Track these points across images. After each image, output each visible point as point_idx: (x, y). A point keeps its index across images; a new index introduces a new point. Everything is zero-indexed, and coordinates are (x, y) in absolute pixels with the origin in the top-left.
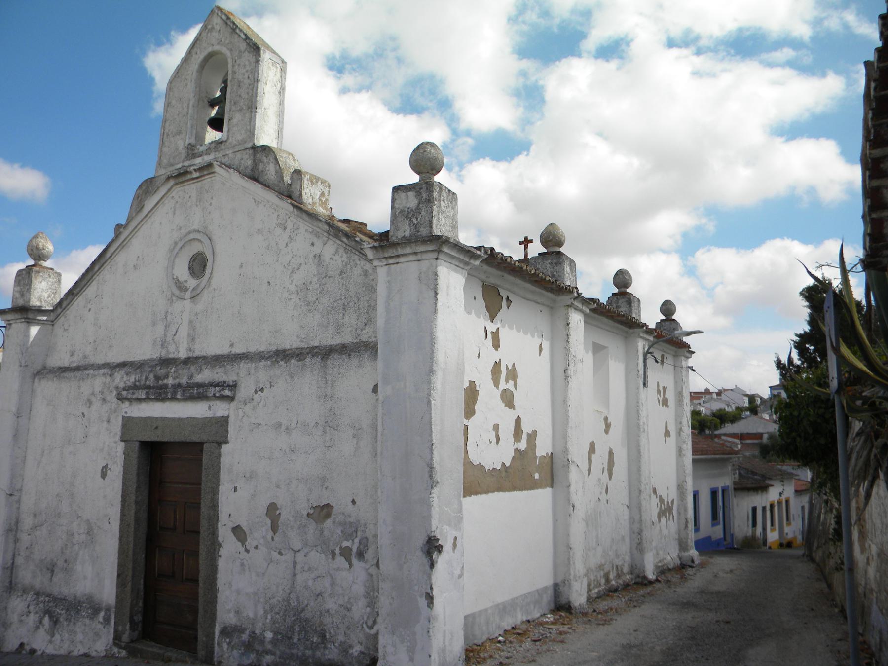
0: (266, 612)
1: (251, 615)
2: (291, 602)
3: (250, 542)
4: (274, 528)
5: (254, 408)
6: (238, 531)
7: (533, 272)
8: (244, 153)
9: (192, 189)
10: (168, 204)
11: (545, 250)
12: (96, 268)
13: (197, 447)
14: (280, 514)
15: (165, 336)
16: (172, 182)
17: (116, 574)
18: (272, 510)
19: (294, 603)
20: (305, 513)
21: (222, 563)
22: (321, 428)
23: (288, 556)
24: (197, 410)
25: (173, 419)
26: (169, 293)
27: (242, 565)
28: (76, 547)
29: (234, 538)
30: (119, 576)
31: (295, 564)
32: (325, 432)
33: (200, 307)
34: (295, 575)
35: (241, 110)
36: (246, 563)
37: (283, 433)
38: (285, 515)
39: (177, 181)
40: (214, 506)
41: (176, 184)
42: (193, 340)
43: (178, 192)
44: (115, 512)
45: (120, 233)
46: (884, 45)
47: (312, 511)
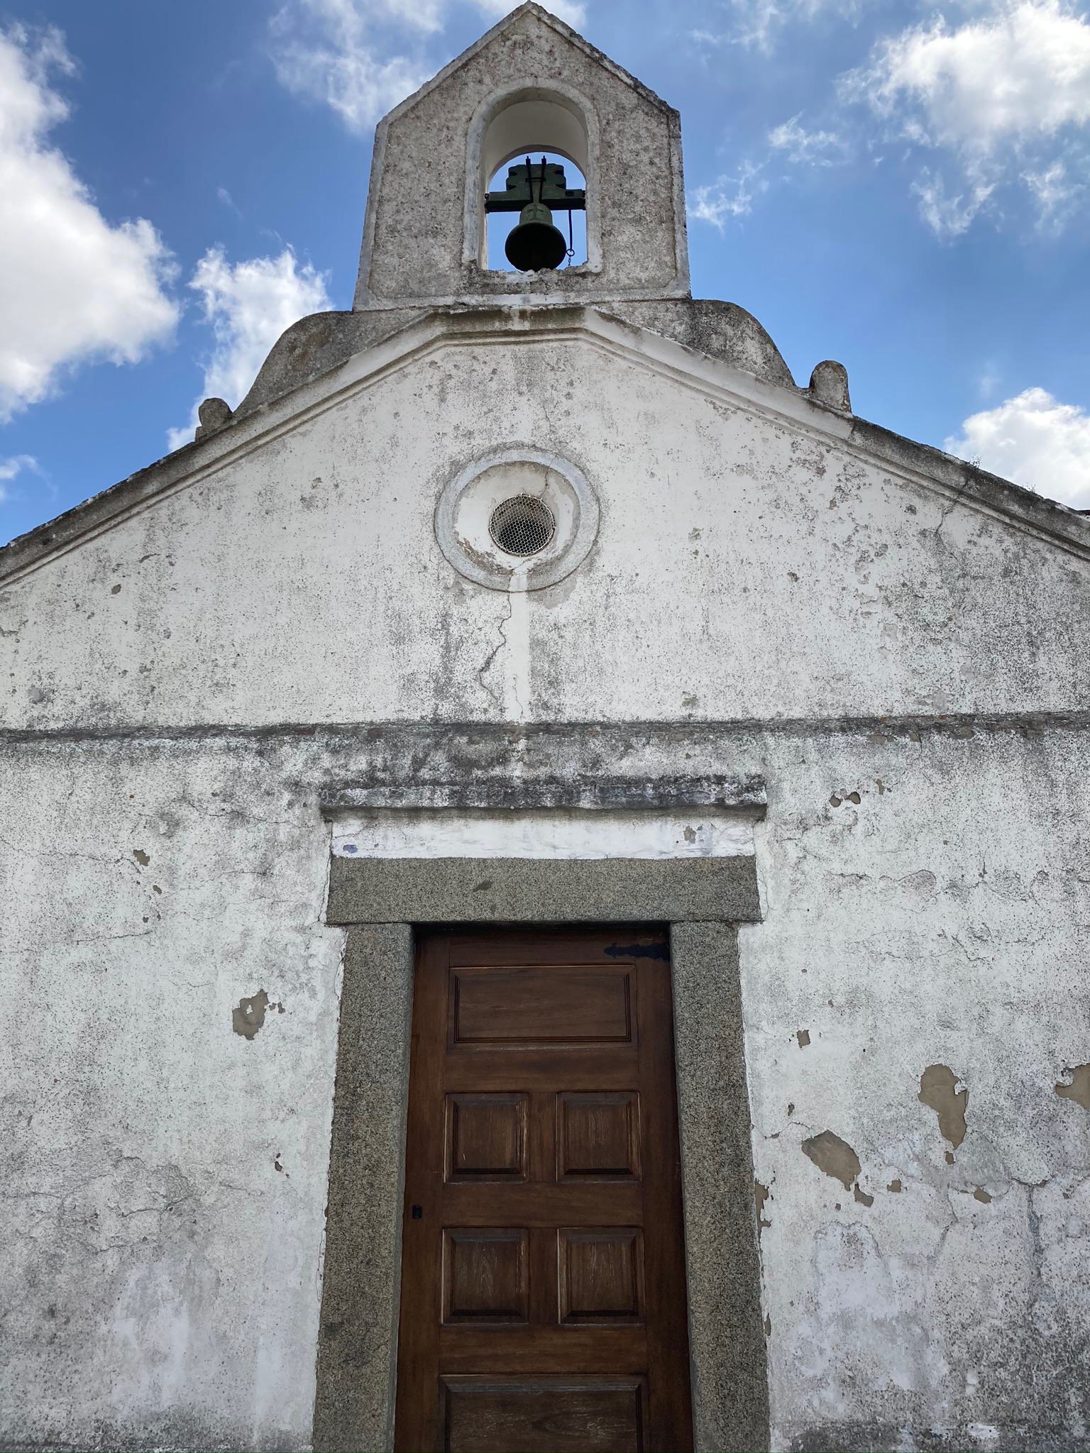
0: (955, 1366)
1: (904, 1382)
2: (1041, 1326)
3: (871, 1175)
4: (953, 1128)
5: (835, 839)
6: (827, 1151)
8: (661, 307)
9: (502, 359)
10: (419, 377)
12: (151, 488)
13: (651, 939)
14: (965, 1091)
16: (439, 329)
17: (312, 1327)
18: (940, 1087)
19: (1049, 1330)
20: (1047, 1085)
21: (773, 1246)
22: (1058, 885)
23: (1012, 1200)
24: (656, 840)
25: (553, 865)
27: (852, 1240)
28: (111, 1260)
29: (813, 1170)
30: (329, 1330)
31: (1035, 1222)
32: (1071, 894)
33: (563, 612)
34: (1039, 1250)
35: (638, 220)
36: (863, 1234)
37: (942, 897)
38: (981, 1094)
39: (456, 329)
40: (732, 1087)
42: (554, 683)
43: (452, 357)
44: (307, 1138)
45: (257, 414)
47: (1068, 1080)
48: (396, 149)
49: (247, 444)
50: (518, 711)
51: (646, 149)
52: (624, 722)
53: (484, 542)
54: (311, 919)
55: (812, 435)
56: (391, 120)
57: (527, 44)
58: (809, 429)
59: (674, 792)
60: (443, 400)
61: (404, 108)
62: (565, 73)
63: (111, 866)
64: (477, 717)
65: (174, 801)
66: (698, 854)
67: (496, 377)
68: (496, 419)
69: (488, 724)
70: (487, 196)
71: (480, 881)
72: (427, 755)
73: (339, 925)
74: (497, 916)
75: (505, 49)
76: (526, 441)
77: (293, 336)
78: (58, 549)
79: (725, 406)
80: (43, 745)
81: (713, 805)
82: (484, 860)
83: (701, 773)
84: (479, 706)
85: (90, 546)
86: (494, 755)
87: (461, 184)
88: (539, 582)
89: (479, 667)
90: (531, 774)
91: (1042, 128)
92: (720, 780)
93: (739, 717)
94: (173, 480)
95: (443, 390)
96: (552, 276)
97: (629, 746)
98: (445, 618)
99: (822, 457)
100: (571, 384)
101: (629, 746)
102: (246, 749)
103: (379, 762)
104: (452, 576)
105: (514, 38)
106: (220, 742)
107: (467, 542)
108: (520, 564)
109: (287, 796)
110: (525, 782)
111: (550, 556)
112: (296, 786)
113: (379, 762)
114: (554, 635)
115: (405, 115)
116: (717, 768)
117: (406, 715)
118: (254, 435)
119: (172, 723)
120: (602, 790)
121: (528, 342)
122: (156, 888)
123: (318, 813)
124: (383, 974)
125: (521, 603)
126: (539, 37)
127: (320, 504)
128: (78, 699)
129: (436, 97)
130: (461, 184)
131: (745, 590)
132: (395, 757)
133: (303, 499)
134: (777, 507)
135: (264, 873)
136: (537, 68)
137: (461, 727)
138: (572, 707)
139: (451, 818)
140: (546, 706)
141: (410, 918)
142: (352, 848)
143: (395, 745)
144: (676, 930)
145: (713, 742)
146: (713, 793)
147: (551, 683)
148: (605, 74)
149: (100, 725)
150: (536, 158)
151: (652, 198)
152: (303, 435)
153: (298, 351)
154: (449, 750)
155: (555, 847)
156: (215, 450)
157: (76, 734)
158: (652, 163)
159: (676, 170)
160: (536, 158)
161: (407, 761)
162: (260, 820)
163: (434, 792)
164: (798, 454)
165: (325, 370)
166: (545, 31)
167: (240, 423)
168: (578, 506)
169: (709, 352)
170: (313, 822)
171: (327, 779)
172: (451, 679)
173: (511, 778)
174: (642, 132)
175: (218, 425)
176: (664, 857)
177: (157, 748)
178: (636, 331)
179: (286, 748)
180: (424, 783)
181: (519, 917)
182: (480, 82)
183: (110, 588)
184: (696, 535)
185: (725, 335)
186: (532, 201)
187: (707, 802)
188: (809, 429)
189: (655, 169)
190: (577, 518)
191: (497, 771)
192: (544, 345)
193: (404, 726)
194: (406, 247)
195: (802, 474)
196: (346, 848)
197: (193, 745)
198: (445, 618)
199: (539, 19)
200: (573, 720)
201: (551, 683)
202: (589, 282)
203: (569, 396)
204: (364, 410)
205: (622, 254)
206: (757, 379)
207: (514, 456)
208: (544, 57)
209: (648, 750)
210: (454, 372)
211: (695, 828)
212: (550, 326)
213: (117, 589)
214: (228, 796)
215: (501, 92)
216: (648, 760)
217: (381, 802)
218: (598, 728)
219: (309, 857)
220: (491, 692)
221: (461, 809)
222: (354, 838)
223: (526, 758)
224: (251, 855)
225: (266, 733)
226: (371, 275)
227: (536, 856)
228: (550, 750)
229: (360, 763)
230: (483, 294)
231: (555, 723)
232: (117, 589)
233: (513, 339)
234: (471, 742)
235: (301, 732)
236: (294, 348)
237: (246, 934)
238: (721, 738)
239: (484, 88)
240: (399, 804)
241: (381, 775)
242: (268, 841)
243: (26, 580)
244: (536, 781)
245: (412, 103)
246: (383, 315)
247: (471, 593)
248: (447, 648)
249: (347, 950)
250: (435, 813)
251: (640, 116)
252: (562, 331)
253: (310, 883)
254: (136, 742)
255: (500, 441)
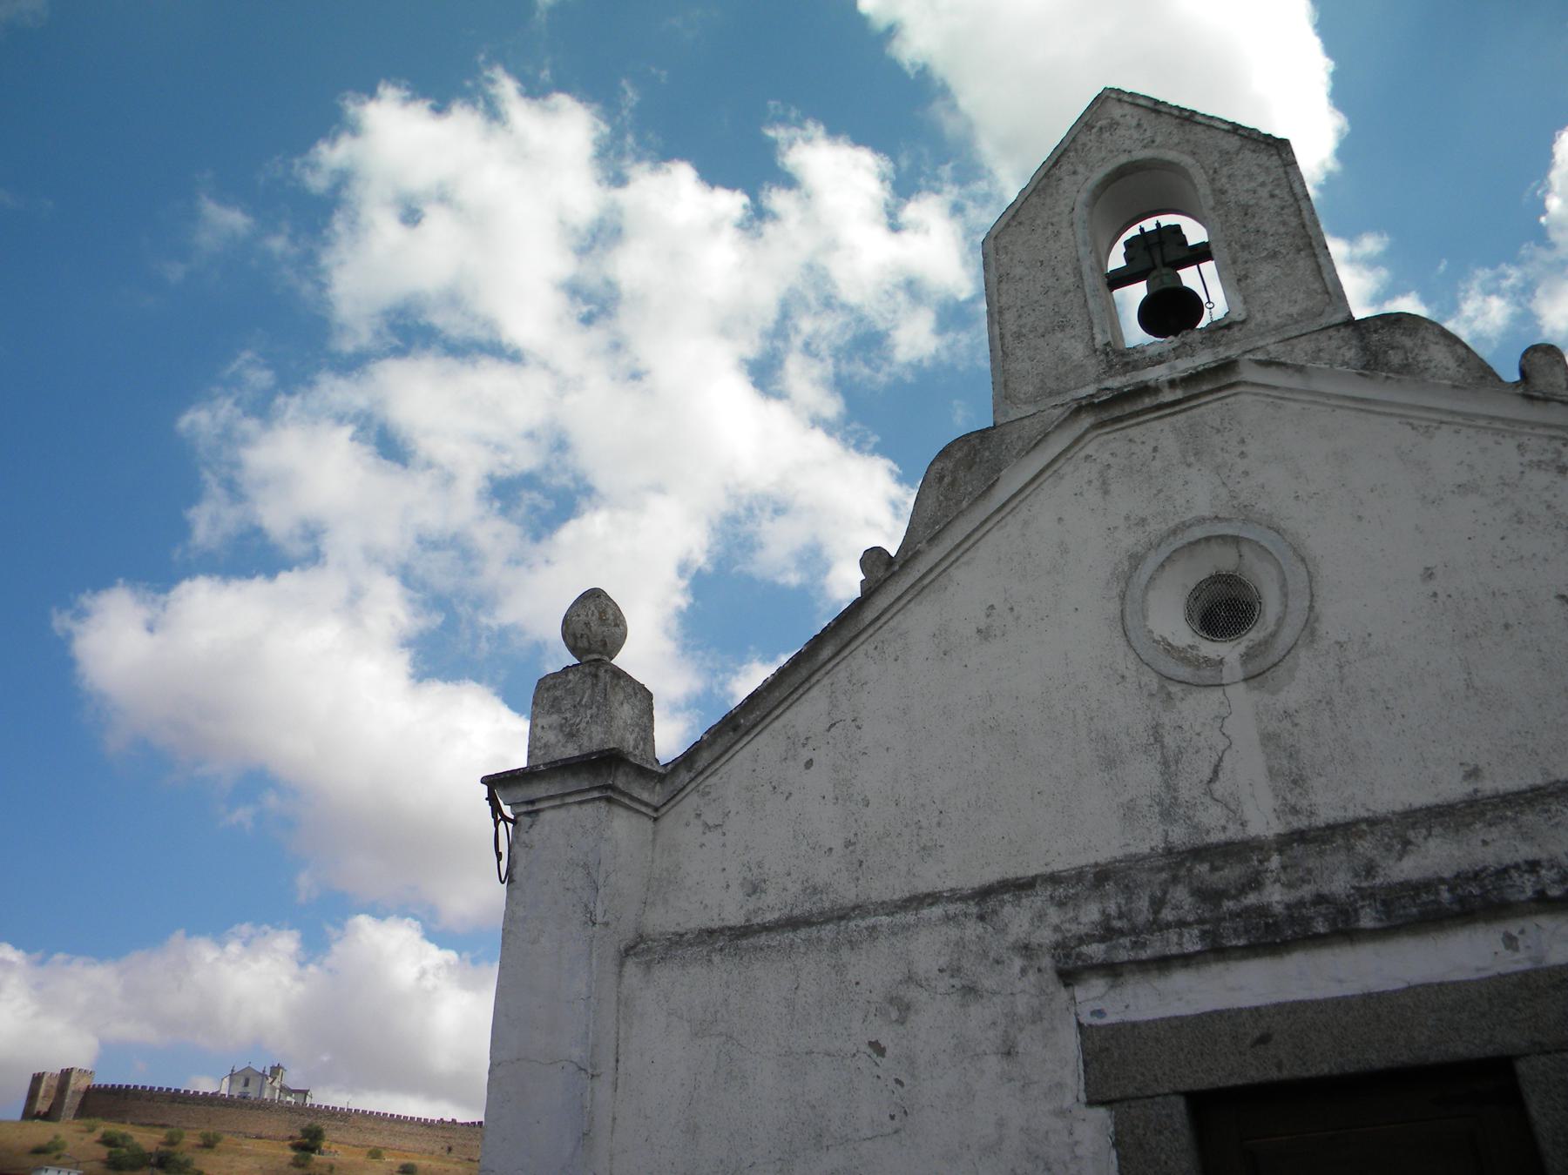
8: (1322, 337)
9: (1161, 434)
12: (826, 653)
15: (1170, 787)
16: (1087, 421)
24: (1465, 955)
26: (1154, 683)
33: (1293, 695)
35: (1274, 255)
39: (1105, 416)
41: (1095, 427)
45: (917, 554)
46: (895, 67)
48: (1004, 258)
49: (912, 586)
50: (1263, 822)
51: (1263, 184)
52: (1394, 813)
53: (1181, 633)
54: (1069, 1101)
55: (1540, 431)
56: (994, 234)
57: (1114, 125)
58: (1534, 425)
59: (1476, 891)
60: (1106, 492)
61: (1004, 220)
62: (1158, 139)
63: (848, 1062)
64: (1216, 837)
65: (901, 982)
66: (1527, 965)
67: (1158, 455)
68: (1168, 498)
69: (1229, 845)
70: (1108, 275)
71: (1257, 1034)
72: (1165, 893)
73: (1102, 1103)
74: (1286, 1074)
75: (1093, 137)
76: (1207, 514)
77: (939, 466)
78: (747, 733)
79: (1424, 423)
80: (763, 939)
81: (1531, 900)
82: (1257, 1009)
83: (1508, 859)
84: (1215, 825)
85: (776, 724)
86: (1244, 880)
87: (1078, 273)
88: (1254, 667)
89: (1206, 779)
90: (1292, 896)
91: (658, 787)
92: (1533, 866)
93: (1539, 781)
94: (846, 639)
95: (1104, 483)
96: (1192, 337)
97: (1406, 843)
98: (1156, 732)
99: (1559, 453)
100: (1243, 441)
101: (1406, 843)
102: (966, 915)
103: (1112, 909)
104: (1155, 680)
105: (1099, 124)
106: (937, 911)
107: (1164, 639)
108: (1229, 651)
109: (1018, 963)
110: (1288, 907)
111: (1262, 635)
112: (1026, 949)
113: (1112, 909)
114: (1287, 724)
115: (1008, 225)
116: (1526, 852)
117: (1133, 850)
118: (918, 575)
119: (886, 898)
120: (1384, 903)
121: (1185, 410)
122: (898, 1082)
123: (1055, 977)
124: (1163, 1157)
125: (1239, 694)
126: (1124, 116)
127: (998, 633)
128: (789, 886)
129: (1034, 200)
130: (1078, 273)
131: (1507, 626)
132: (1129, 900)
133: (979, 631)
134: (1520, 522)
135: (1009, 1053)
136: (1130, 145)
137: (1198, 853)
138: (1327, 807)
139: (1207, 962)
140: (1295, 811)
141: (1182, 1087)
142: (1099, 1013)
143: (1127, 886)
144: (1522, 1067)
145: (1514, 820)
146: (1526, 886)
147: (1295, 782)
148: (1199, 128)
149: (815, 910)
150: (1149, 225)
151: (1282, 230)
152: (968, 563)
153: (947, 480)
154: (1190, 883)
155: (1340, 981)
156: (882, 601)
157: (793, 923)
158: (1272, 196)
159: (1300, 196)
160: (1149, 225)
161: (1143, 904)
162: (994, 993)
163: (1181, 935)
164: (1528, 457)
165: (976, 494)
166: (1127, 109)
167: (901, 567)
168: (1282, 572)
169: (1390, 370)
170: (1051, 988)
171: (1058, 936)
172: (1176, 799)
173: (1270, 904)
174: (1255, 170)
175: (881, 574)
176: (1484, 974)
177: (874, 927)
178: (1300, 369)
179: (1008, 909)
180: (1168, 925)
181: (1313, 1072)
182: (1075, 173)
183: (802, 765)
184: (1429, 574)
185: (1403, 347)
186: (1154, 267)
187: (1523, 897)
188: (1534, 425)
189: (1277, 201)
190: (1284, 585)
191: (1251, 899)
192: (1203, 409)
193: (1134, 860)
194: (1036, 348)
195: (1540, 479)
196: (1093, 1013)
197: (910, 918)
198: (1156, 732)
199: (1119, 100)
200: (1331, 821)
201: (1295, 782)
202: (1235, 332)
203: (1243, 455)
204: (1026, 523)
205: (1265, 295)
206: (1454, 387)
207: (1198, 533)
208: (1133, 131)
209: (1432, 843)
210: (1112, 460)
211: (1515, 932)
212: (1205, 388)
213: (809, 764)
214: (956, 971)
215: (1098, 175)
216: (1435, 857)
217: (1123, 956)
218: (1364, 827)
219: (1054, 1029)
220: (1226, 806)
221: (1217, 951)
222: (1093, 995)
223: (1283, 878)
224: (991, 1034)
225: (984, 894)
226: (1006, 386)
227: (1318, 994)
228: (1310, 863)
229: (1091, 913)
230: (1125, 373)
231: (1310, 829)
232: (809, 764)
233: (1168, 411)
234: (1213, 869)
235: (1020, 887)
236: (941, 478)
237: (1001, 1124)
238: (1522, 812)
239: (1080, 178)
240: (1144, 955)
241: (1117, 924)
242: (1006, 1015)
243: (723, 770)
244: (1301, 903)
245: (1011, 213)
246: (1026, 422)
247: (1180, 694)
248: (1166, 763)
249: (1116, 1133)
250: (1186, 960)
251: (1247, 154)
252: (1219, 389)
253: (1059, 1060)
254: (852, 924)
255: (1177, 521)
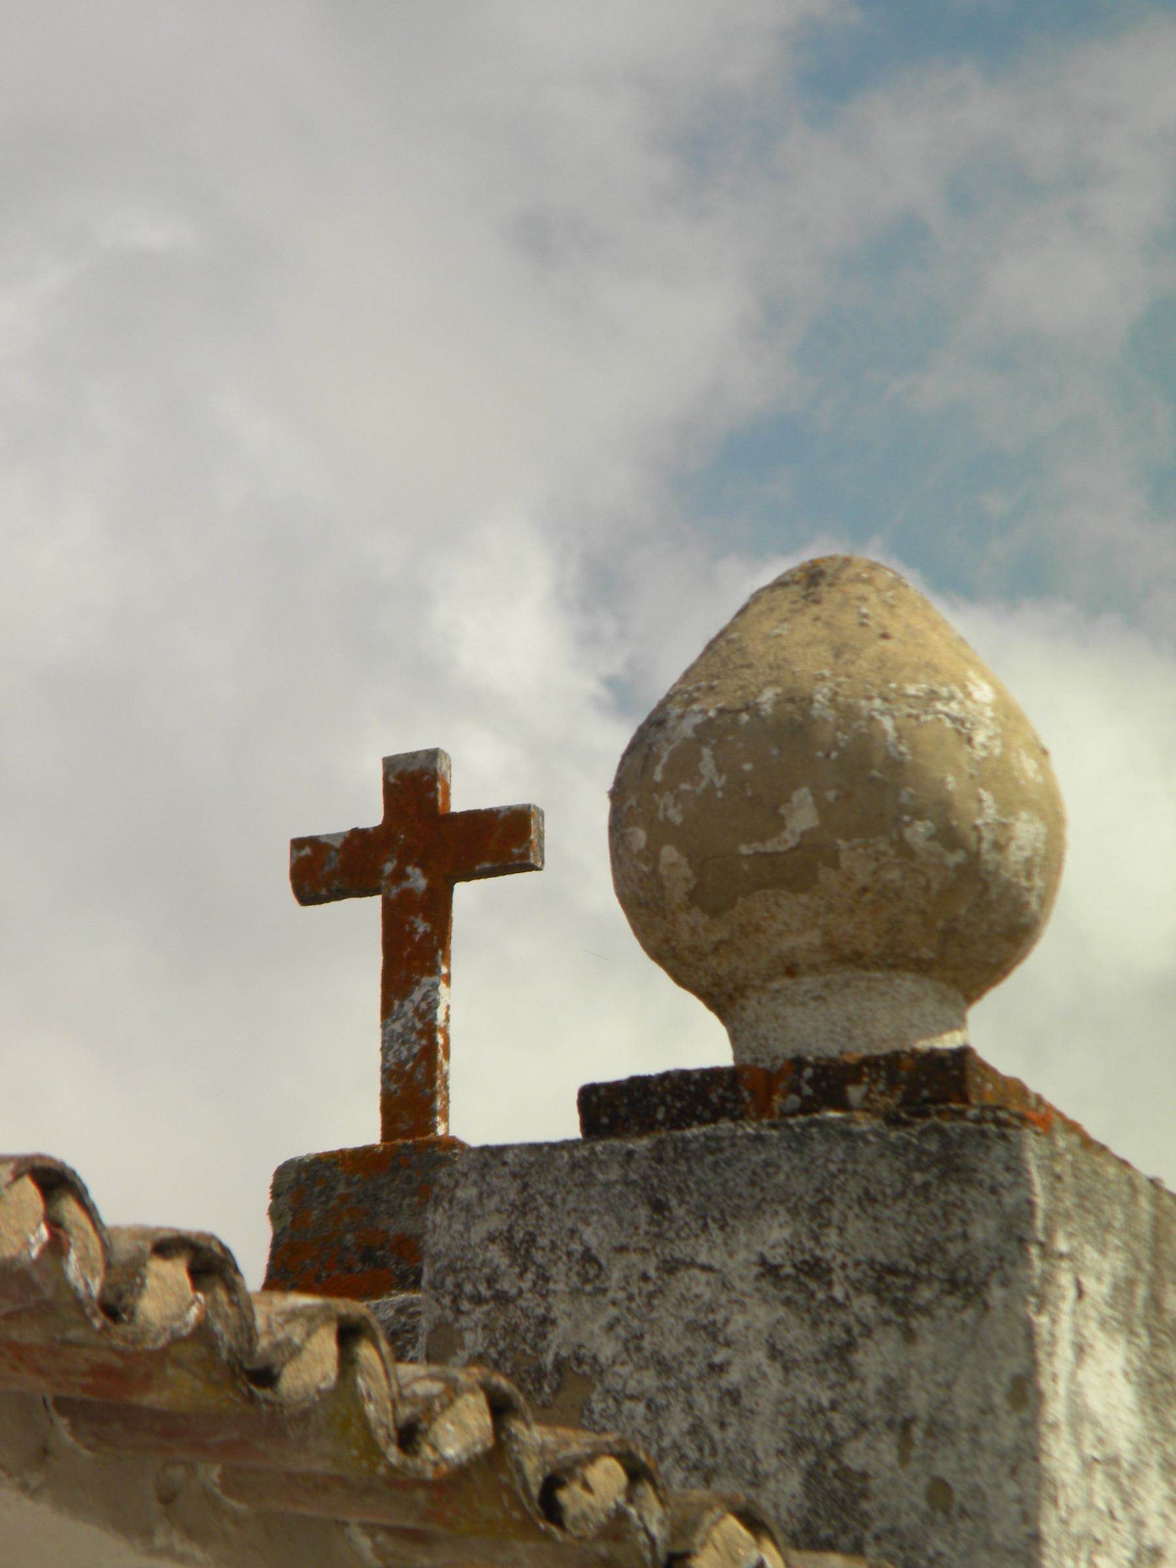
7: (460, 1433)
11: (701, 1042)
